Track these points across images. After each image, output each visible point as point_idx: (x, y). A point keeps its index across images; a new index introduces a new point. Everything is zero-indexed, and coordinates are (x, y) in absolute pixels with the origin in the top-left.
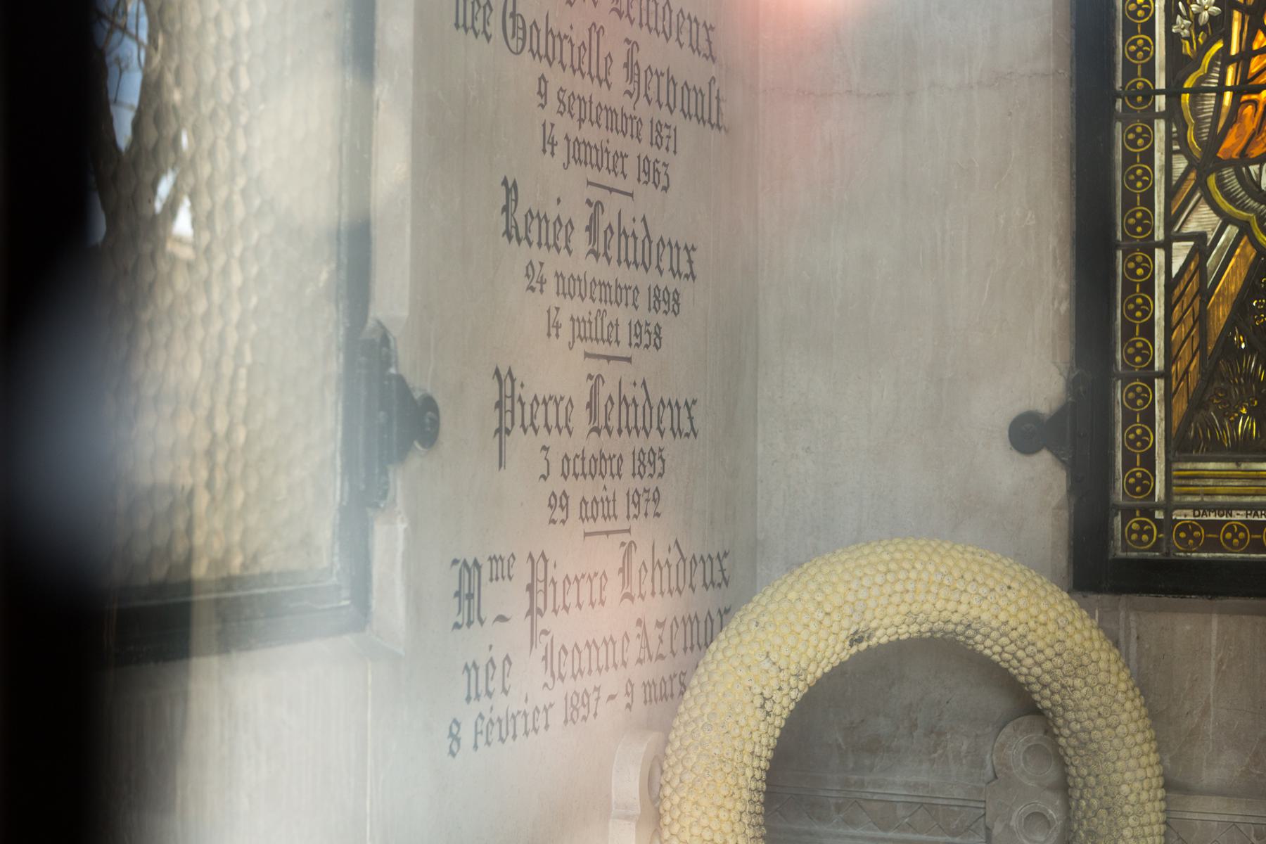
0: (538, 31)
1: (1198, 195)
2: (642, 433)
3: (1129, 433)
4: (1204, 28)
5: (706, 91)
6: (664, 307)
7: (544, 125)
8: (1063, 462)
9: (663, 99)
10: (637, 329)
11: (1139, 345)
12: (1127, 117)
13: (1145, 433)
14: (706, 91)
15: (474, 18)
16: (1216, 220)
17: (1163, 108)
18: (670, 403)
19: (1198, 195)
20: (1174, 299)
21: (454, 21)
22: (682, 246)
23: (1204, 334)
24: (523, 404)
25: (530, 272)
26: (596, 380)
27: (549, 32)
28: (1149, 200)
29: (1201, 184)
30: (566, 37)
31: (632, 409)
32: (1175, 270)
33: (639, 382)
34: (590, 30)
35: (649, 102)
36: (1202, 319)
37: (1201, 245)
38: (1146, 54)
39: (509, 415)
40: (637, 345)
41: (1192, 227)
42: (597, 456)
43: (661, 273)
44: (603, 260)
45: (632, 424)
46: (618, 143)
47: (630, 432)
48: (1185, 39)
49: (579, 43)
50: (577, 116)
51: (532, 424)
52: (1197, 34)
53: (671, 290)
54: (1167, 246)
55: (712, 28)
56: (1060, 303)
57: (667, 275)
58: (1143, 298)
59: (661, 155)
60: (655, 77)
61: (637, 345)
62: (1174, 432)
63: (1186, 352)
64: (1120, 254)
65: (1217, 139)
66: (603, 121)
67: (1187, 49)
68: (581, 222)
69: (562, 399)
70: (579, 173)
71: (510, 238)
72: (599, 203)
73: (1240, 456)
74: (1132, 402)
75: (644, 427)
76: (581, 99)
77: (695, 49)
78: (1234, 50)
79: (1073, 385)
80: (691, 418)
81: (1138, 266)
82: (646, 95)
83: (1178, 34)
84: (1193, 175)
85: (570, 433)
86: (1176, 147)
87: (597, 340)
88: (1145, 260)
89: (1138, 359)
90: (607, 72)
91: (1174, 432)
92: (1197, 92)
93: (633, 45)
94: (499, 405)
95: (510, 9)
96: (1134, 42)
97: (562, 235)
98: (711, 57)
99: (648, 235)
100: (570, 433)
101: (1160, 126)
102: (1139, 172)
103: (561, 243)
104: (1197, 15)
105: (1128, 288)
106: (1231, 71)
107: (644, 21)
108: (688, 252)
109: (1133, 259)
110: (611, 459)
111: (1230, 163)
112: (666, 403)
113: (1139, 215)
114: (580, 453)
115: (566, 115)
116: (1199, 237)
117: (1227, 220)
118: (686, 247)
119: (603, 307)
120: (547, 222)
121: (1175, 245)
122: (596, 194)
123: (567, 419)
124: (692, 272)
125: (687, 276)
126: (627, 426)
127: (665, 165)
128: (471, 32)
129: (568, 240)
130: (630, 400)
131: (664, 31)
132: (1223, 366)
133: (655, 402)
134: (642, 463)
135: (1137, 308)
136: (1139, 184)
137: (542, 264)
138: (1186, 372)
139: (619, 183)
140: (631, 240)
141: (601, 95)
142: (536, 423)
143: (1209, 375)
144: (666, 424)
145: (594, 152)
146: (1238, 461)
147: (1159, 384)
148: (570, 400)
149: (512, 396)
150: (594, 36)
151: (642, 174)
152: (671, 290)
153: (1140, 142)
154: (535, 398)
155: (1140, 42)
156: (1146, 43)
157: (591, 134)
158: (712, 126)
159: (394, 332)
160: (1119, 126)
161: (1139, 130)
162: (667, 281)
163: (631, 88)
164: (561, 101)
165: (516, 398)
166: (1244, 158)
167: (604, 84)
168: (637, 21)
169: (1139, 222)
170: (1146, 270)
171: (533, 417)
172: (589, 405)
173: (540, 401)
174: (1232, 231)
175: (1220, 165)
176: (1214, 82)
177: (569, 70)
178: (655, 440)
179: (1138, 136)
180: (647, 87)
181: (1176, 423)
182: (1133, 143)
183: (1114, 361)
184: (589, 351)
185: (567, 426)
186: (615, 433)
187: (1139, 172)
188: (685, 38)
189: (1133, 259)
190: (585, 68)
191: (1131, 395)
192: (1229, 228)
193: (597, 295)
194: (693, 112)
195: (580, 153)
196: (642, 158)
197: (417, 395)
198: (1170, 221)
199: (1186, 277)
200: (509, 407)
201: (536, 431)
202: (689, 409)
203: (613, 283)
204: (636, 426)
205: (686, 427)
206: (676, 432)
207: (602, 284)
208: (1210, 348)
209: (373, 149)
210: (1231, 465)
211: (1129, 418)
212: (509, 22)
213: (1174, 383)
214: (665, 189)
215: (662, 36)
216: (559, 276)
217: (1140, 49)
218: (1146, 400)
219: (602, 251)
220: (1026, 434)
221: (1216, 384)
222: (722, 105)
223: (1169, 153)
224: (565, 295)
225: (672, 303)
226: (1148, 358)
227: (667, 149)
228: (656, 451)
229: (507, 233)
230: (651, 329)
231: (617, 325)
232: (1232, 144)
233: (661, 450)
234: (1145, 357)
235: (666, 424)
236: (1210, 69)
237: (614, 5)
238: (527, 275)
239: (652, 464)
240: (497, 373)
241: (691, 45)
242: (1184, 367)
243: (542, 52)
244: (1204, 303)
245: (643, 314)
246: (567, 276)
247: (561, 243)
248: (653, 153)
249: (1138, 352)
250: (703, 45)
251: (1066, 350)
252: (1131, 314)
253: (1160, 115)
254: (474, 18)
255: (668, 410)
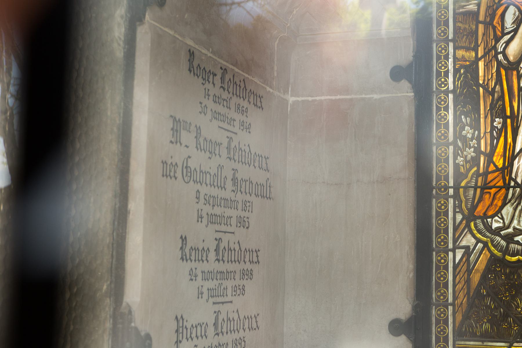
0: (196, 172)
1: (467, 230)
2: (236, 332)
3: (438, 328)
4: (469, 162)
5: (265, 185)
6: (246, 277)
7: (198, 211)
8: (411, 340)
9: (247, 191)
10: (235, 288)
11: (442, 291)
12: (438, 197)
13: (445, 328)
14: (265, 185)
15: (170, 171)
16: (473, 241)
17: (452, 194)
18: (248, 317)
19: (467, 230)
20: (457, 273)
21: (162, 174)
22: (254, 250)
23: (469, 288)
24: (187, 329)
25: (191, 273)
26: (217, 313)
27: (201, 171)
28: (446, 231)
29: (468, 226)
30: (208, 172)
31: (232, 323)
32: (457, 261)
33: (235, 311)
34: (218, 168)
35: (242, 193)
36: (468, 282)
37: (468, 252)
38: (445, 171)
39: (181, 335)
40: (235, 295)
41: (464, 243)
42: (217, 345)
43: (245, 263)
44: (221, 262)
45: (232, 329)
46: (229, 212)
47: (231, 332)
48: (462, 165)
49: (213, 174)
50: (212, 205)
51: (191, 337)
52: (466, 163)
53: (249, 270)
54: (454, 251)
55: (268, 158)
56: (410, 273)
57: (248, 263)
58: (445, 79)
59: (246, 214)
60: (244, 182)
61: (235, 295)
62: (456, 328)
63: (461, 295)
64: (434, 253)
65: (474, 207)
66: (222, 205)
67: (462, 170)
68: (213, 248)
69: (203, 324)
70: (213, 227)
71: (183, 260)
72: (220, 239)
73: (484, 339)
74: (439, 315)
75: (237, 329)
76: (214, 197)
77: (261, 168)
78: (481, 171)
79: (415, 308)
80: (256, 322)
81: (442, 258)
82: (240, 190)
83: (459, 163)
84: (464, 222)
85: (206, 337)
86: (458, 210)
87: (218, 296)
88: (445, 256)
89: (442, 297)
90: (225, 184)
91: (456, 328)
92: (466, 188)
93: (235, 170)
94: (177, 331)
95: (185, 165)
96: (440, 166)
97: (205, 255)
98: (267, 170)
99: (240, 248)
100: (206, 337)
101: (451, 201)
102: (442, 220)
103: (204, 258)
104: (466, 156)
105: (438, 268)
106: (480, 179)
107: (240, 160)
108: (257, 252)
109: (440, 256)
110: (223, 345)
111: (479, 217)
112: (246, 317)
113: (442, 237)
114: (210, 345)
115: (208, 205)
116: (467, 248)
117: (478, 241)
118: (256, 251)
119: (220, 282)
120: (199, 251)
121: (457, 250)
122: (219, 235)
123: (205, 332)
124: (258, 261)
125: (256, 263)
126: (230, 330)
127: (248, 218)
128: (169, 177)
129: (207, 256)
130: (231, 319)
131: (248, 163)
132: (476, 301)
133: (242, 317)
134: (236, 344)
135: (442, 276)
136: (442, 225)
137: (196, 269)
138: (462, 303)
139: (229, 229)
140: (233, 252)
141: (222, 194)
142: (192, 336)
143: (471, 305)
144: (246, 326)
145: (218, 218)
146: (483, 342)
147: (450, 308)
148: (207, 324)
149: (183, 326)
150: (220, 170)
151: (238, 224)
152: (249, 270)
153: (443, 207)
154: (192, 325)
155: (443, 166)
156: (445, 167)
157: (217, 211)
158: (267, 198)
159: (134, 308)
160: (434, 200)
161: (442, 202)
162: (248, 266)
163: (234, 189)
164: (205, 199)
165: (184, 327)
166: (485, 216)
167: (223, 189)
168: (237, 161)
169: (442, 241)
170: (445, 261)
171: (191, 333)
172: (214, 324)
173: (194, 326)
174: (480, 245)
175: (475, 218)
176: (473, 184)
177: (209, 186)
178: (242, 334)
179: (442, 205)
180: (241, 187)
181: (457, 325)
182: (440, 208)
183: (432, 298)
184: (215, 301)
185: (205, 335)
186: (225, 334)
187: (442, 220)
188: (257, 164)
189: (440, 256)
190: (215, 184)
191: (439, 312)
192: (479, 244)
193: (218, 277)
194: (259, 194)
195: (213, 219)
196: (238, 216)
197: (143, 334)
198: (455, 241)
199: (462, 264)
200: (181, 331)
201: (192, 339)
202: (256, 318)
203: (225, 271)
204: (234, 329)
205: (254, 326)
206: (251, 329)
207: (221, 272)
208: (471, 294)
209: (127, 231)
210: (480, 343)
211: (438, 322)
212: (185, 170)
213: (457, 308)
214: (247, 228)
215: (247, 165)
216: (203, 272)
217: (443, 169)
218: (445, 315)
219: (221, 258)
220: (397, 73)
221: (474, 309)
222: (272, 189)
223: (455, 213)
224: (205, 280)
225: (249, 275)
226: (446, 297)
227: (249, 211)
228: (242, 338)
229: (182, 258)
230: (241, 287)
231: (227, 288)
232: (480, 210)
233: (244, 338)
234: (445, 297)
235: (246, 326)
236: (471, 179)
237: (228, 156)
238: (190, 274)
239: (240, 344)
240: (177, 318)
241: (259, 166)
242: (461, 301)
243: (198, 180)
244: (469, 275)
245: (238, 282)
246: (206, 271)
247: (204, 258)
248: (243, 214)
249: (442, 294)
250: (264, 165)
251: (412, 292)
252: (439, 278)
253: (451, 197)
254: (170, 171)
255: (247, 320)
